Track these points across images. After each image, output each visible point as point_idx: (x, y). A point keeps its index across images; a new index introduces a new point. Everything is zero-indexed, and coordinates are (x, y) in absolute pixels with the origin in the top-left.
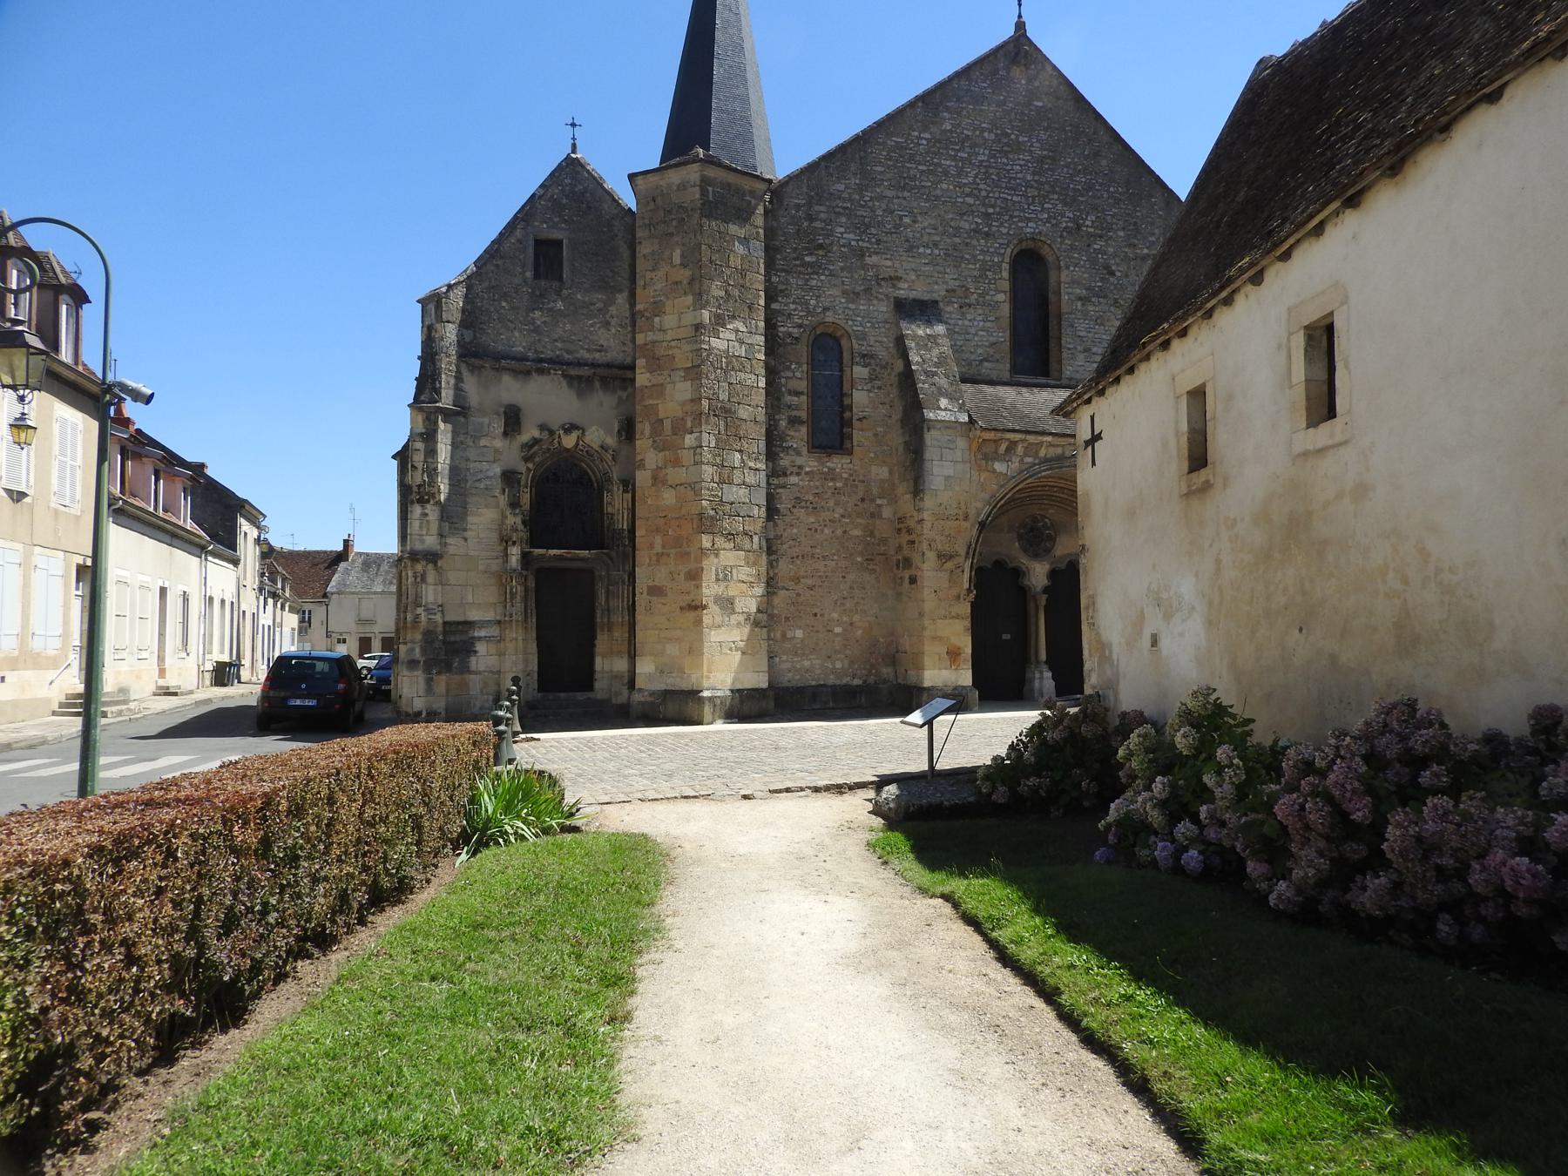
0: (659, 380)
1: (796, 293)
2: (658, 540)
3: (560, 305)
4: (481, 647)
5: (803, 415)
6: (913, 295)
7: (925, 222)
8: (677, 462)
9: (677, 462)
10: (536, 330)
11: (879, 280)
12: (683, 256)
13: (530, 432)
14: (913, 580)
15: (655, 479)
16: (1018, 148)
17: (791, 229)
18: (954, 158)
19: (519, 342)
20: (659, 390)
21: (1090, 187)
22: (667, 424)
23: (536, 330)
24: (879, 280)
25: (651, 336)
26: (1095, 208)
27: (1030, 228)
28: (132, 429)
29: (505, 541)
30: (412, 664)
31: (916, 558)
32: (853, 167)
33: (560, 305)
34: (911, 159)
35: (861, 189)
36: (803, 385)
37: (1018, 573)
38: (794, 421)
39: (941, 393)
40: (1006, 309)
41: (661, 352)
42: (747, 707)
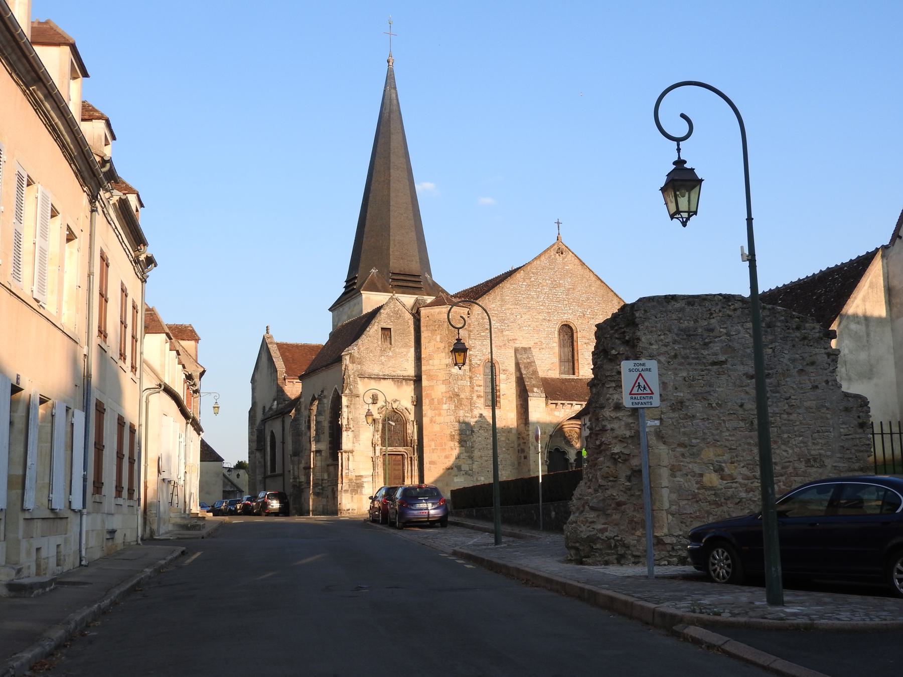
0: (432, 384)
1: (479, 347)
2: (433, 444)
3: (391, 354)
4: (365, 485)
5: (482, 394)
6: (521, 346)
7: (525, 317)
8: (440, 415)
9: (440, 415)
10: (383, 364)
11: (509, 340)
12: (441, 338)
13: (381, 403)
14: (525, 458)
15: (431, 421)
16: (560, 285)
17: (476, 323)
18: (536, 292)
19: (376, 369)
20: (432, 387)
21: (588, 299)
22: (436, 400)
23: (383, 364)
24: (509, 340)
25: (428, 367)
26: (590, 307)
27: (565, 317)
28: (514, 432)
29: (374, 446)
30: (346, 491)
31: (526, 450)
32: (498, 298)
33: (391, 354)
34: (520, 293)
35: (501, 306)
36: (482, 383)
37: (564, 453)
38: (478, 397)
39: (534, 386)
40: (557, 349)
41: (432, 373)
42: (849, 275)
